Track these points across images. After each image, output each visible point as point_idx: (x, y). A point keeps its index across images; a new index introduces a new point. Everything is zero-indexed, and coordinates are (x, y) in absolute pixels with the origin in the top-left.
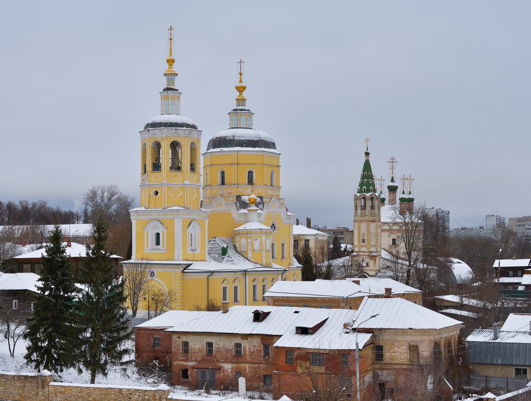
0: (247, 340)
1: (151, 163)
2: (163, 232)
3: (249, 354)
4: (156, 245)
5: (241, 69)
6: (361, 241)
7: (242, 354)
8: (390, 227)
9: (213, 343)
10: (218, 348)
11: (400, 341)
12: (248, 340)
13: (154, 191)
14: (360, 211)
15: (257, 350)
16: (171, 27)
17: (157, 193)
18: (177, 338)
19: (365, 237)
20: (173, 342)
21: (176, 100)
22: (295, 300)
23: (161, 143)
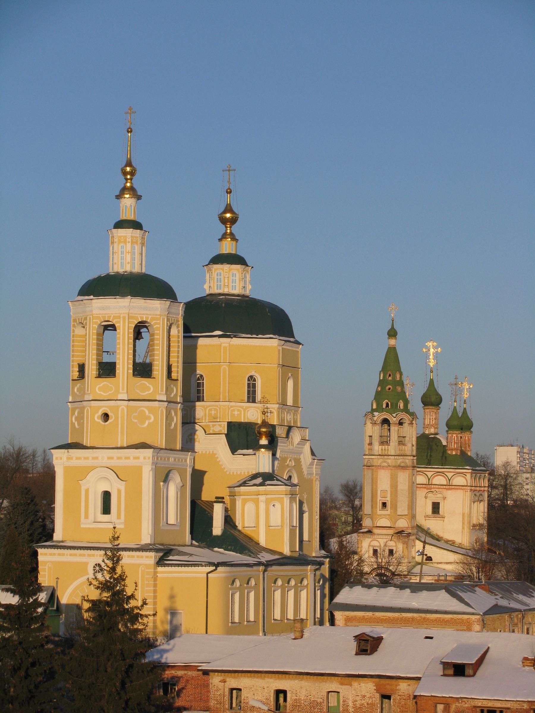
0: (351, 686)
1: (96, 361)
2: (119, 491)
3: (353, 710)
4: (101, 514)
5: (229, 182)
6: (379, 505)
7: (341, 710)
8: (429, 480)
9: (286, 691)
10: (296, 700)
11: (438, 705)
12: (351, 685)
13: (100, 412)
14: (378, 446)
15: (368, 704)
16: (130, 109)
17: (106, 417)
18: (220, 682)
19: (386, 499)
20: (212, 689)
21: (127, 244)
22: (388, 618)
23: (116, 326)
